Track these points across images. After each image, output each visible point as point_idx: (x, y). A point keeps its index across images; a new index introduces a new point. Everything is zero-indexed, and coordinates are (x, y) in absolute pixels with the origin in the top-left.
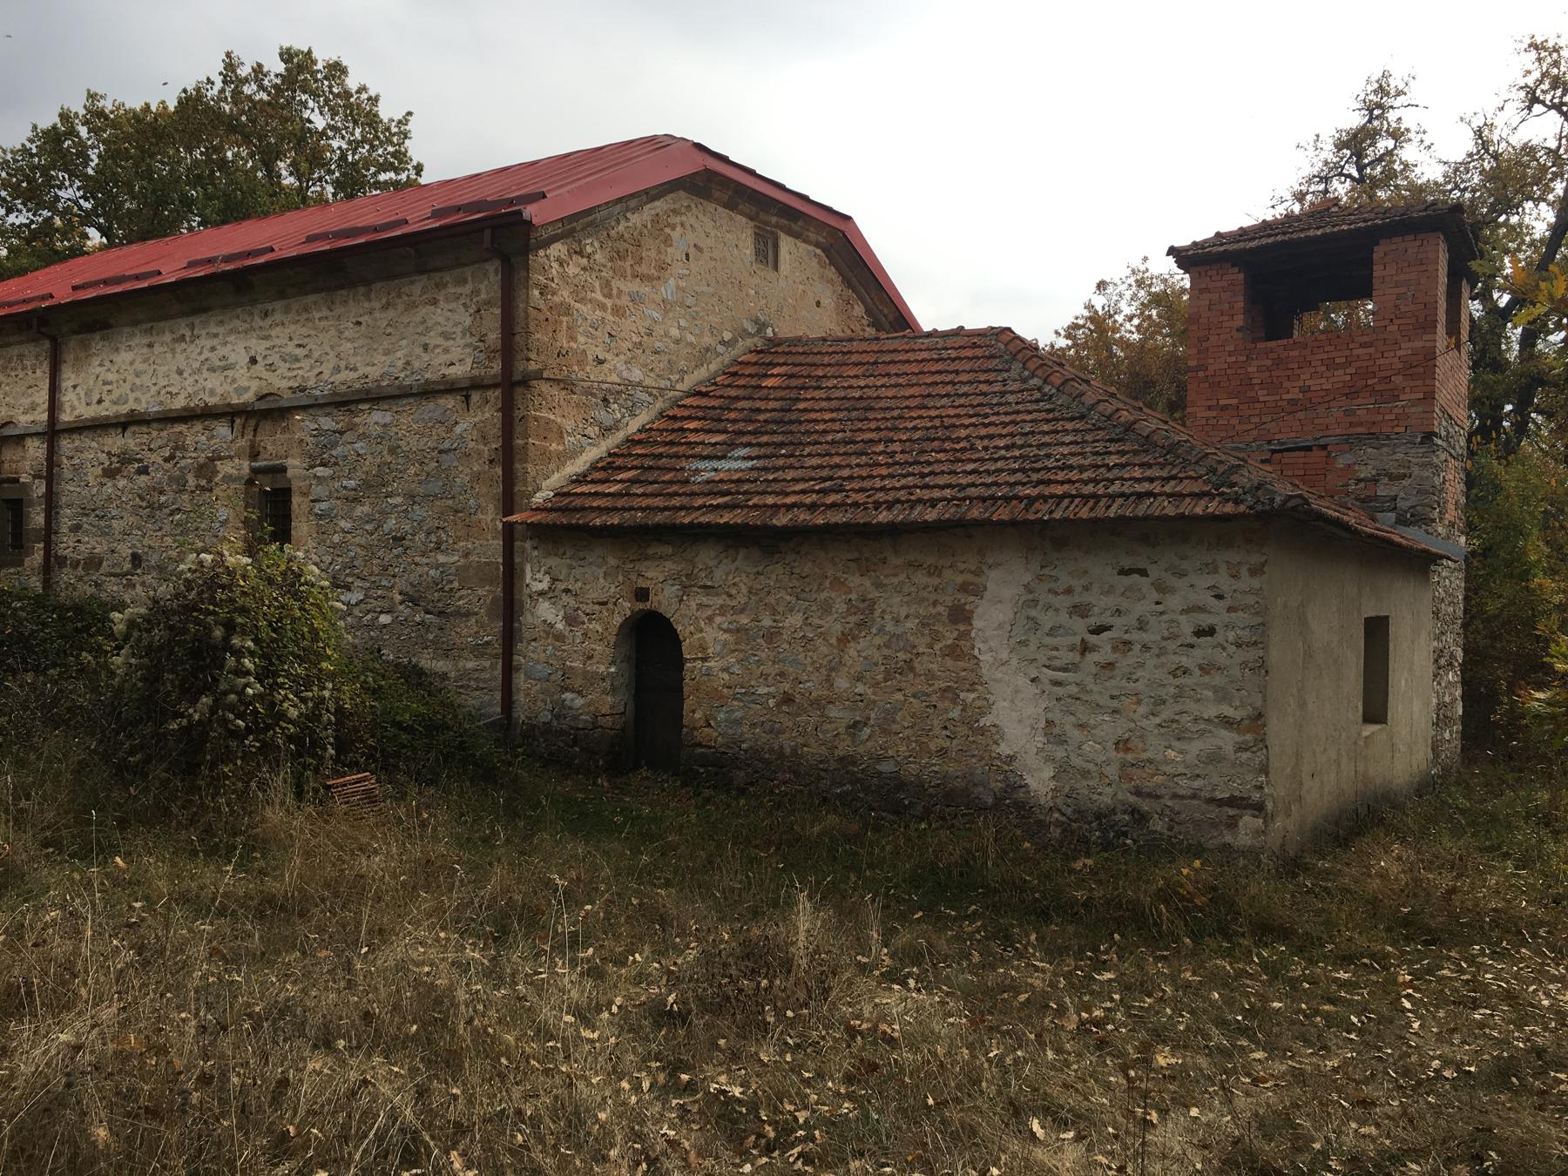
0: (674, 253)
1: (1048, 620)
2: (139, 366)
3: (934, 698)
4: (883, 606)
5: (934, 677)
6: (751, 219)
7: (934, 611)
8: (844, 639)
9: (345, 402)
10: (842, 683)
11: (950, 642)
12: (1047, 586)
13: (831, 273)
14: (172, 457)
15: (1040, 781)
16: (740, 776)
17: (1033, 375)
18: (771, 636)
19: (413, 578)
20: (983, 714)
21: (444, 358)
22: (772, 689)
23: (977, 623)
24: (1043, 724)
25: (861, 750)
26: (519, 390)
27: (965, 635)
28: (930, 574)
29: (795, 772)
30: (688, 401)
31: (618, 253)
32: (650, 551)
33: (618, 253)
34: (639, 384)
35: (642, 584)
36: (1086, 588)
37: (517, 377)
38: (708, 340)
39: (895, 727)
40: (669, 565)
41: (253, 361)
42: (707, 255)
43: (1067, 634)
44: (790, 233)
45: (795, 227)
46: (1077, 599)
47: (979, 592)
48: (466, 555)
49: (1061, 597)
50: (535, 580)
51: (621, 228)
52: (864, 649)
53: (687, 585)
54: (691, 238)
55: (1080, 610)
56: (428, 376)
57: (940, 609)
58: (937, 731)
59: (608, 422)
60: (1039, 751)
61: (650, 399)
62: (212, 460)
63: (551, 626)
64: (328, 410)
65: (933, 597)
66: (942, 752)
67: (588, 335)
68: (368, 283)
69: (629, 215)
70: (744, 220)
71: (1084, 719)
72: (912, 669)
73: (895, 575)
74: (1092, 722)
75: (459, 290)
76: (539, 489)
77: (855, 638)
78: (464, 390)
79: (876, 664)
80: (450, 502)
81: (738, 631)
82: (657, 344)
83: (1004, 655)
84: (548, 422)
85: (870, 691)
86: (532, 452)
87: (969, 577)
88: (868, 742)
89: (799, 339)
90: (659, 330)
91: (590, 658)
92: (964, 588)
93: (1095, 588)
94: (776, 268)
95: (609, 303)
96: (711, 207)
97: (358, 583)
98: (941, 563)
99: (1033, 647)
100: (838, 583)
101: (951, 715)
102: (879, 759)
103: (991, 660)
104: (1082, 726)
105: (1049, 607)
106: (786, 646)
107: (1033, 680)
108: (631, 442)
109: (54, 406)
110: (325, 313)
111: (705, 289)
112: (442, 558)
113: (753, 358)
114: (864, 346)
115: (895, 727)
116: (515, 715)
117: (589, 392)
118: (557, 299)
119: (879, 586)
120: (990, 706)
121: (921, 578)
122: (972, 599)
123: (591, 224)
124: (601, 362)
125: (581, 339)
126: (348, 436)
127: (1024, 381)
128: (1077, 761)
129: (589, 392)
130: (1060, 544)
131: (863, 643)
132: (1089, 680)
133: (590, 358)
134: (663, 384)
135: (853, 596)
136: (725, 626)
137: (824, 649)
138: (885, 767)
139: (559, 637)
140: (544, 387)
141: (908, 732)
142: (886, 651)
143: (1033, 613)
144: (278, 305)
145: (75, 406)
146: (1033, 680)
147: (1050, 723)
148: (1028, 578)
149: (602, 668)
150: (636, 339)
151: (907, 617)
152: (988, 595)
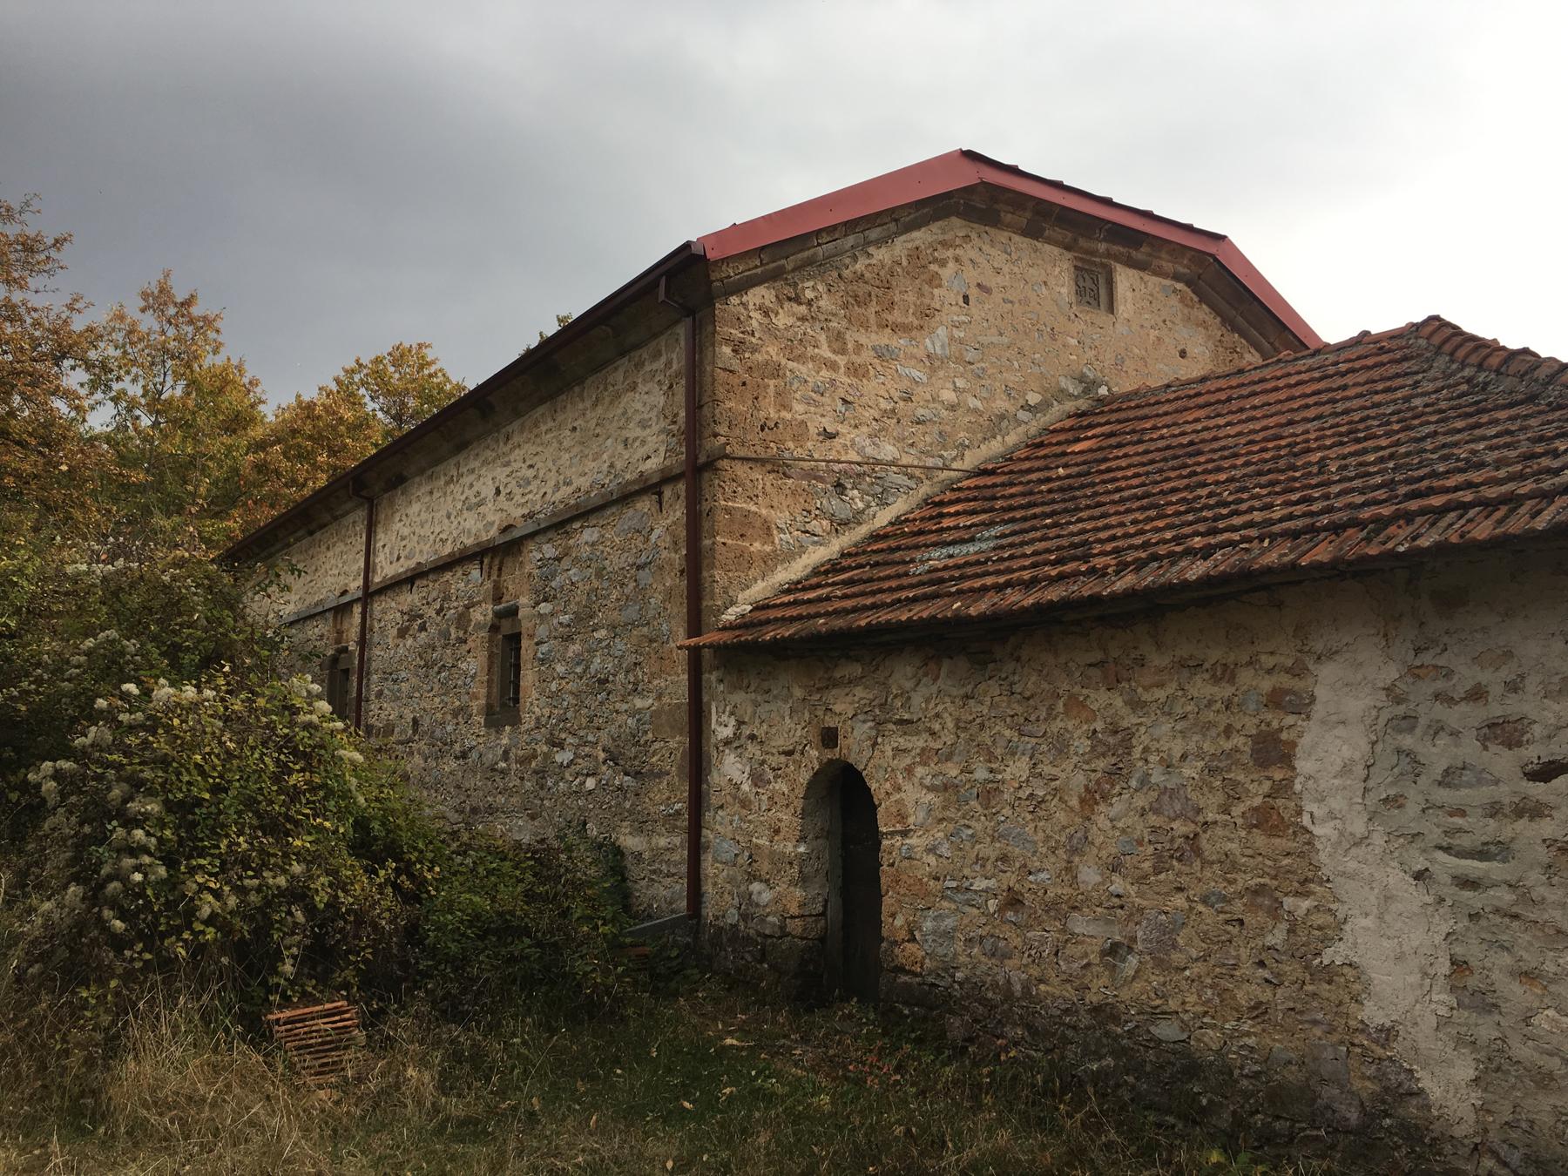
0: (945, 295)
1: (1439, 754)
2: (424, 516)
3: (1238, 906)
4: (1146, 739)
5: (1235, 867)
6: (1068, 248)
7: (1228, 745)
8: (1092, 798)
9: (562, 523)
10: (1089, 875)
11: (1258, 801)
12: (1427, 688)
13: (1203, 313)
14: (442, 609)
15: (1449, 1087)
16: (956, 1026)
17: (1463, 366)
18: (989, 793)
19: (613, 729)
20: (1327, 941)
21: (642, 452)
22: (992, 883)
23: (1304, 765)
24: (1444, 967)
25: (1125, 994)
26: (706, 475)
27: (1282, 789)
28: (1216, 680)
29: (1029, 1027)
30: (965, 484)
31: (856, 297)
32: (837, 675)
33: (856, 297)
34: (893, 463)
35: (830, 722)
36: (1513, 687)
37: (702, 459)
38: (1001, 404)
39: (1177, 958)
40: (859, 692)
41: (498, 492)
42: (997, 296)
43: (1480, 782)
44: (1131, 263)
45: (1138, 255)
46: (1495, 710)
47: (1302, 706)
48: (659, 697)
49: (1463, 708)
50: (722, 728)
51: (859, 266)
52: (1120, 816)
53: (883, 719)
54: (971, 275)
55: (1504, 732)
56: (628, 477)
57: (1238, 740)
58: (1247, 969)
59: (844, 513)
60: (1442, 1023)
61: (912, 484)
62: (467, 607)
63: (737, 787)
64: (550, 535)
65: (1223, 720)
66: (1259, 1011)
67: (809, 402)
68: (580, 381)
69: (871, 250)
70: (1056, 251)
71: (1531, 960)
72: (1198, 852)
73: (1161, 685)
74: (1550, 967)
75: (655, 366)
76: (733, 603)
77: (1105, 797)
78: (652, 487)
79: (1140, 842)
80: (645, 629)
81: (945, 788)
82: (921, 411)
83: (1358, 827)
84: (747, 514)
85: (1132, 890)
86: (721, 555)
87: (1286, 681)
88: (1134, 985)
89: (1136, 393)
90: (922, 394)
91: (777, 832)
92: (1276, 700)
93: (1532, 684)
94: (1111, 309)
95: (841, 361)
96: (1003, 236)
97: (570, 740)
98: (1231, 658)
99: (1412, 809)
100: (1076, 705)
101: (1270, 940)
102: (1156, 1015)
103: (1334, 836)
104: (1528, 976)
105: (1437, 729)
106: (1007, 811)
107: (1419, 876)
108: (875, 537)
109: (368, 569)
110: (550, 424)
111: (995, 339)
112: (639, 703)
113: (1068, 423)
114: (1222, 383)
115: (1177, 958)
116: (704, 912)
117: (812, 475)
118: (759, 357)
119: (1136, 705)
120: (1340, 925)
121: (1201, 687)
122: (1290, 720)
123: (810, 262)
124: (831, 436)
125: (799, 407)
126: (566, 563)
127: (1447, 376)
128: (1522, 1051)
129: (812, 475)
130: (1450, 602)
131: (1118, 806)
132: (1535, 877)
133: (813, 431)
134: (930, 462)
135: (1099, 725)
136: (927, 781)
137: (1061, 816)
138: (1166, 1031)
139: (745, 804)
140: (741, 470)
141: (1197, 969)
142: (1153, 819)
143: (1407, 741)
144: (516, 425)
145: (386, 568)
146: (1419, 876)
147: (1459, 966)
148: (1392, 673)
149: (790, 848)
150: (884, 405)
151: (1184, 757)
152: (1318, 710)
